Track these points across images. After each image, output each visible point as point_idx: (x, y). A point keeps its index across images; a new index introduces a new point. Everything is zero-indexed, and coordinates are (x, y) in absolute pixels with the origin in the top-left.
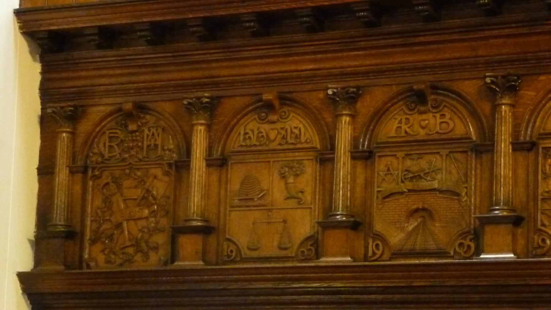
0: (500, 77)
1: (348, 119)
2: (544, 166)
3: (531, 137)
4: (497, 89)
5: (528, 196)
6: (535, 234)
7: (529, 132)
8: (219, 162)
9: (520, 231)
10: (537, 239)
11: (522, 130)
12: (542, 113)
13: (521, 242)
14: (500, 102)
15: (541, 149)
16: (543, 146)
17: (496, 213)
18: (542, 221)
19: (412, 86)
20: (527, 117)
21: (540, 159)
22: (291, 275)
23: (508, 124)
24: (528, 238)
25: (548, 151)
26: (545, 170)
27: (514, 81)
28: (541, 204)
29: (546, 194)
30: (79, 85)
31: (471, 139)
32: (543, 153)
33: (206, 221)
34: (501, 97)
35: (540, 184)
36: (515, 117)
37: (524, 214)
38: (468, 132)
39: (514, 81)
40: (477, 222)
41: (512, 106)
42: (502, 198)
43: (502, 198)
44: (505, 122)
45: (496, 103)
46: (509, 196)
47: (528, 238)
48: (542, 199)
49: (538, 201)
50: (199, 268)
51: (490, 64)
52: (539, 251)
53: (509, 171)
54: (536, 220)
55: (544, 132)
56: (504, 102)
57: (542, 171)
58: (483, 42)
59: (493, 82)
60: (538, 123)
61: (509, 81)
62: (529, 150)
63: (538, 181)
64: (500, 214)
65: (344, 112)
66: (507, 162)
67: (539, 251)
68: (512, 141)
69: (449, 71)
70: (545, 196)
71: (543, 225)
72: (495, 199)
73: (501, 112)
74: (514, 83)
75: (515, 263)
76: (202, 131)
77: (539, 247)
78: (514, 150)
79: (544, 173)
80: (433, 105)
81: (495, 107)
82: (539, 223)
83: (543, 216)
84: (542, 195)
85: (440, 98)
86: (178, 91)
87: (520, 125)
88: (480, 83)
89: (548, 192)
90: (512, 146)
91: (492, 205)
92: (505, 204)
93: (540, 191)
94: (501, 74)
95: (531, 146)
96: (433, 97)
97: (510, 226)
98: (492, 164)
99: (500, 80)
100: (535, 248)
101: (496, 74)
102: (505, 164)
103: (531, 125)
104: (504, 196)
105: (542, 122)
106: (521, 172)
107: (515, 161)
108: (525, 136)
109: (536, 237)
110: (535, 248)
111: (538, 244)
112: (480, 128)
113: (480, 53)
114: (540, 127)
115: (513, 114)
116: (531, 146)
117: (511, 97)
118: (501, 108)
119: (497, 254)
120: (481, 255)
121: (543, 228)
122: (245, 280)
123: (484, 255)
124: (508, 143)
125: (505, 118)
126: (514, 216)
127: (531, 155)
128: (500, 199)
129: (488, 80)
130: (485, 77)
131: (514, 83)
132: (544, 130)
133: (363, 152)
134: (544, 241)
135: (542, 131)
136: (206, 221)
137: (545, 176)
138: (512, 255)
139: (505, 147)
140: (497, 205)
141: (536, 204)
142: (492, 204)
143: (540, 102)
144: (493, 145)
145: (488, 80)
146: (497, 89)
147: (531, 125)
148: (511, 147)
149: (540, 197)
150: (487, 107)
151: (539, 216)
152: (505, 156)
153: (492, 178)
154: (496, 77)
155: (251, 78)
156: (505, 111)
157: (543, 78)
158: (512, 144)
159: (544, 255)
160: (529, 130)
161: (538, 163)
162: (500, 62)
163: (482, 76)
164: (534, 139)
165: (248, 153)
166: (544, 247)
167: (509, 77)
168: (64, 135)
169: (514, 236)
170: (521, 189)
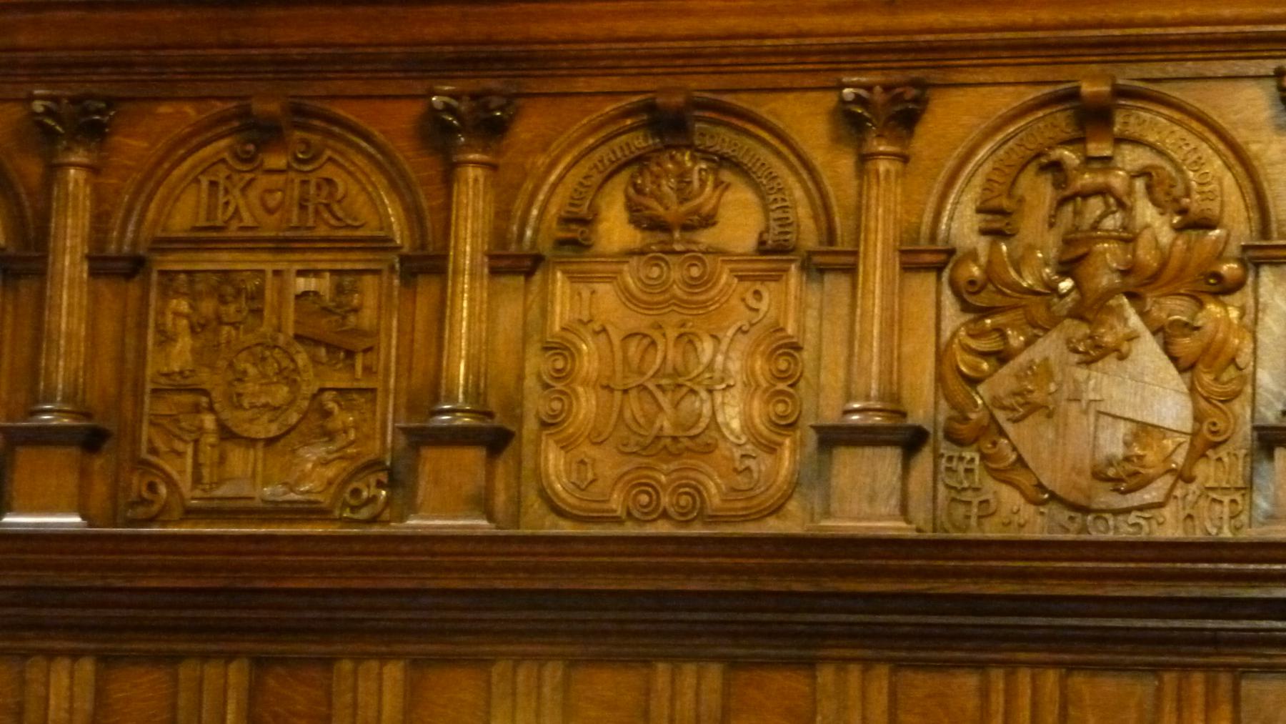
0: (878, 89)
1: (480, 172)
2: (161, 313)
3: (135, 243)
4: (58, 128)
5: (121, 382)
6: (133, 470)
7: (130, 235)
8: (528, 263)
9: (98, 463)
10: (137, 483)
11: (113, 230)
12: (162, 191)
13: (100, 489)
14: (66, 160)
15: (155, 276)
16: (160, 268)
17: (444, 421)
18: (150, 441)
19: (654, 99)
20: (126, 198)
21: (153, 295)
22: (1232, 566)
23: (80, 213)
24: (117, 481)
25: (171, 280)
26: (164, 324)
27: (99, 112)
28: (151, 403)
29: (163, 380)
30: (624, 34)
31: (392, 240)
32: (160, 284)
33: (87, 415)
34: (68, 149)
35: (149, 358)
36: (98, 197)
37: (111, 426)
38: (384, 223)
39: (99, 112)
40: (402, 441)
41: (93, 170)
42: (60, 386)
43: (60, 386)
44: (75, 207)
45: (55, 161)
46: (76, 380)
47: (117, 481)
48: (154, 391)
49: (143, 394)
50: (479, 532)
51: (43, 69)
52: (141, 512)
53: (79, 324)
54: (136, 441)
55: (163, 235)
56: (73, 159)
57: (157, 326)
58: (30, 16)
59: (48, 112)
60: (151, 215)
61: (86, 112)
62: (129, 276)
63: (145, 348)
64: (55, 423)
65: (471, 157)
66: (76, 300)
67: (141, 512)
68: (489, 249)
69: (270, 76)
70: (160, 384)
71: (154, 451)
72: (45, 386)
73: (67, 183)
74: (97, 117)
75: (492, 539)
76: (481, 180)
77: (143, 501)
78: (94, 273)
79: (160, 330)
80: (300, 156)
81: (53, 170)
82: (144, 446)
83: (153, 430)
84: (153, 381)
85: (315, 138)
86: (1049, 60)
87: (108, 214)
88: (830, 99)
89: (167, 375)
90: (900, 257)
91: (37, 402)
92: (66, 399)
93: (149, 372)
94: (68, 93)
95: (134, 267)
96: (298, 134)
97: (75, 451)
98: (41, 303)
99: (879, 96)
100: (133, 505)
101: (56, 93)
102: (70, 305)
103: (134, 219)
104: (64, 381)
105: (160, 212)
106: (108, 327)
107: (95, 298)
108: (121, 242)
109: (135, 480)
110: (133, 505)
111: (140, 496)
112: (414, 214)
113: (22, 40)
114: (155, 223)
115: (96, 189)
116: (134, 267)
117: (89, 150)
118: (67, 173)
119: (45, 516)
120: (407, 519)
121: (153, 459)
122: (672, 570)
123: (10, 516)
124: (78, 256)
125: (76, 198)
126: (86, 428)
127: (133, 289)
128: (56, 388)
129: (38, 106)
130: (32, 98)
131: (97, 117)
132: (164, 230)
133: (519, 257)
134: (152, 487)
135: (159, 234)
136: (87, 415)
137: (163, 338)
138: (77, 519)
139: (72, 264)
140: (47, 401)
141: (138, 402)
142: (33, 401)
143: (159, 163)
144: (44, 258)
145: (38, 106)
146: (58, 128)
147: (134, 219)
148: (86, 267)
149: (149, 387)
150: (32, 169)
151: (146, 431)
152: (71, 287)
153: (39, 335)
154: (869, 88)
155: (841, 44)
156: (76, 182)
157: (164, 109)
158: (90, 258)
159: (150, 521)
160: (131, 228)
161: (148, 305)
162: (66, 66)
163: (23, 95)
164: (141, 252)
165: (229, 246)
166: (151, 502)
167: (88, 102)
168: (72, 171)
169: (84, 473)
170: (106, 370)
